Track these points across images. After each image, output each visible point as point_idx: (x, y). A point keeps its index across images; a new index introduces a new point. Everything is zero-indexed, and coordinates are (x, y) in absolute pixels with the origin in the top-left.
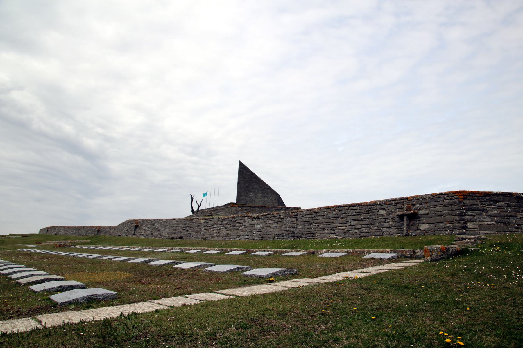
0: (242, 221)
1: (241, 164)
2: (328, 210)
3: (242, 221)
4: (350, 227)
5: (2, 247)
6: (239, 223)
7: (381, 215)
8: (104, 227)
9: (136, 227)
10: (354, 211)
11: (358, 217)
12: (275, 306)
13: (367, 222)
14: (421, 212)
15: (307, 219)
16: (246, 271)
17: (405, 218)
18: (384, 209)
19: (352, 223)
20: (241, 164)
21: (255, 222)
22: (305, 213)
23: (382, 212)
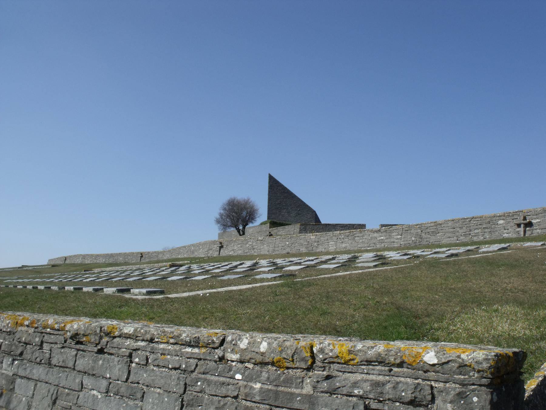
0: (362, 235)
1: (271, 178)
2: (452, 222)
3: (362, 235)
4: (473, 235)
5: (544, 231)
6: (358, 237)
7: (500, 224)
8: (149, 253)
9: (142, 257)
10: (477, 222)
11: (481, 226)
12: (248, 293)
13: (489, 230)
14: (533, 221)
15: (432, 230)
16: (275, 277)
17: (522, 226)
18: (503, 219)
19: (476, 231)
20: (271, 178)
21: (376, 235)
22: (429, 225)
23: (501, 222)
